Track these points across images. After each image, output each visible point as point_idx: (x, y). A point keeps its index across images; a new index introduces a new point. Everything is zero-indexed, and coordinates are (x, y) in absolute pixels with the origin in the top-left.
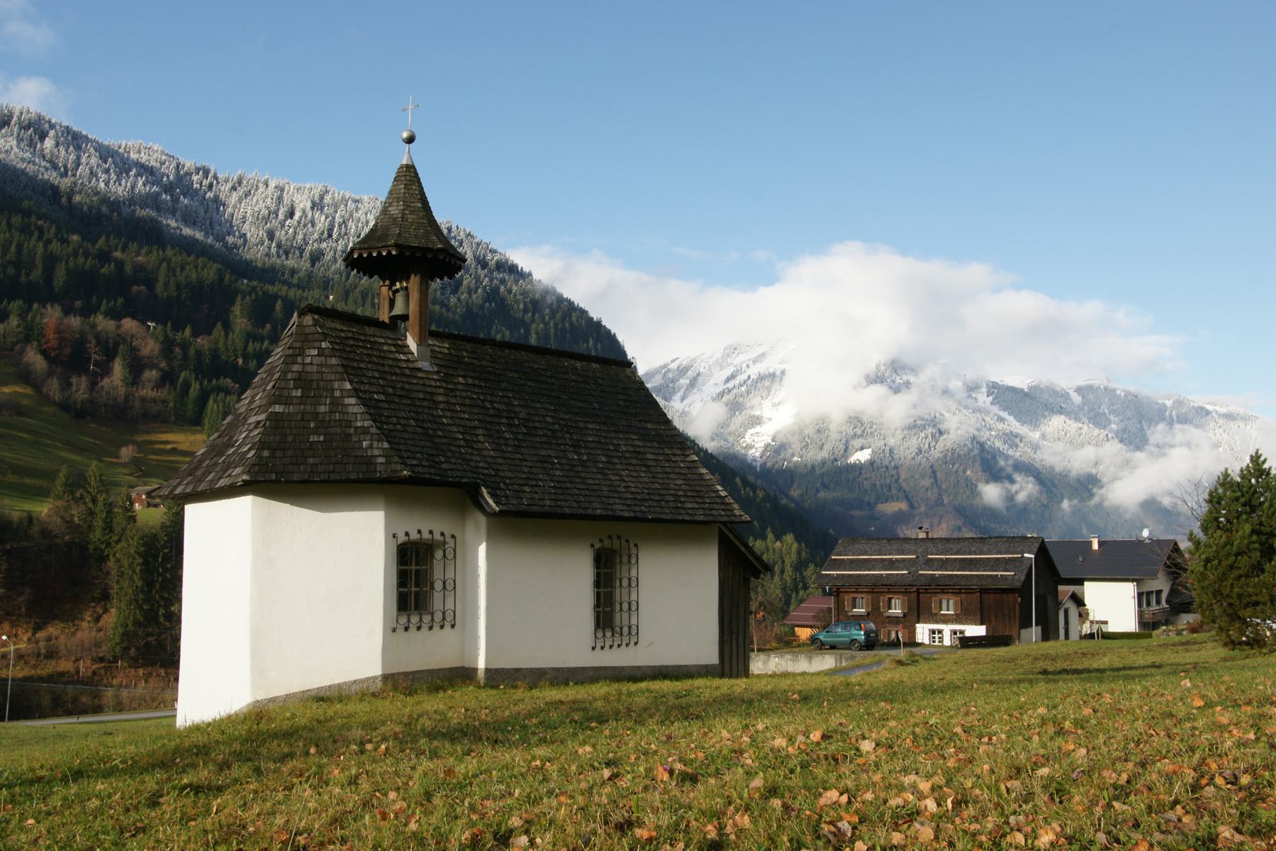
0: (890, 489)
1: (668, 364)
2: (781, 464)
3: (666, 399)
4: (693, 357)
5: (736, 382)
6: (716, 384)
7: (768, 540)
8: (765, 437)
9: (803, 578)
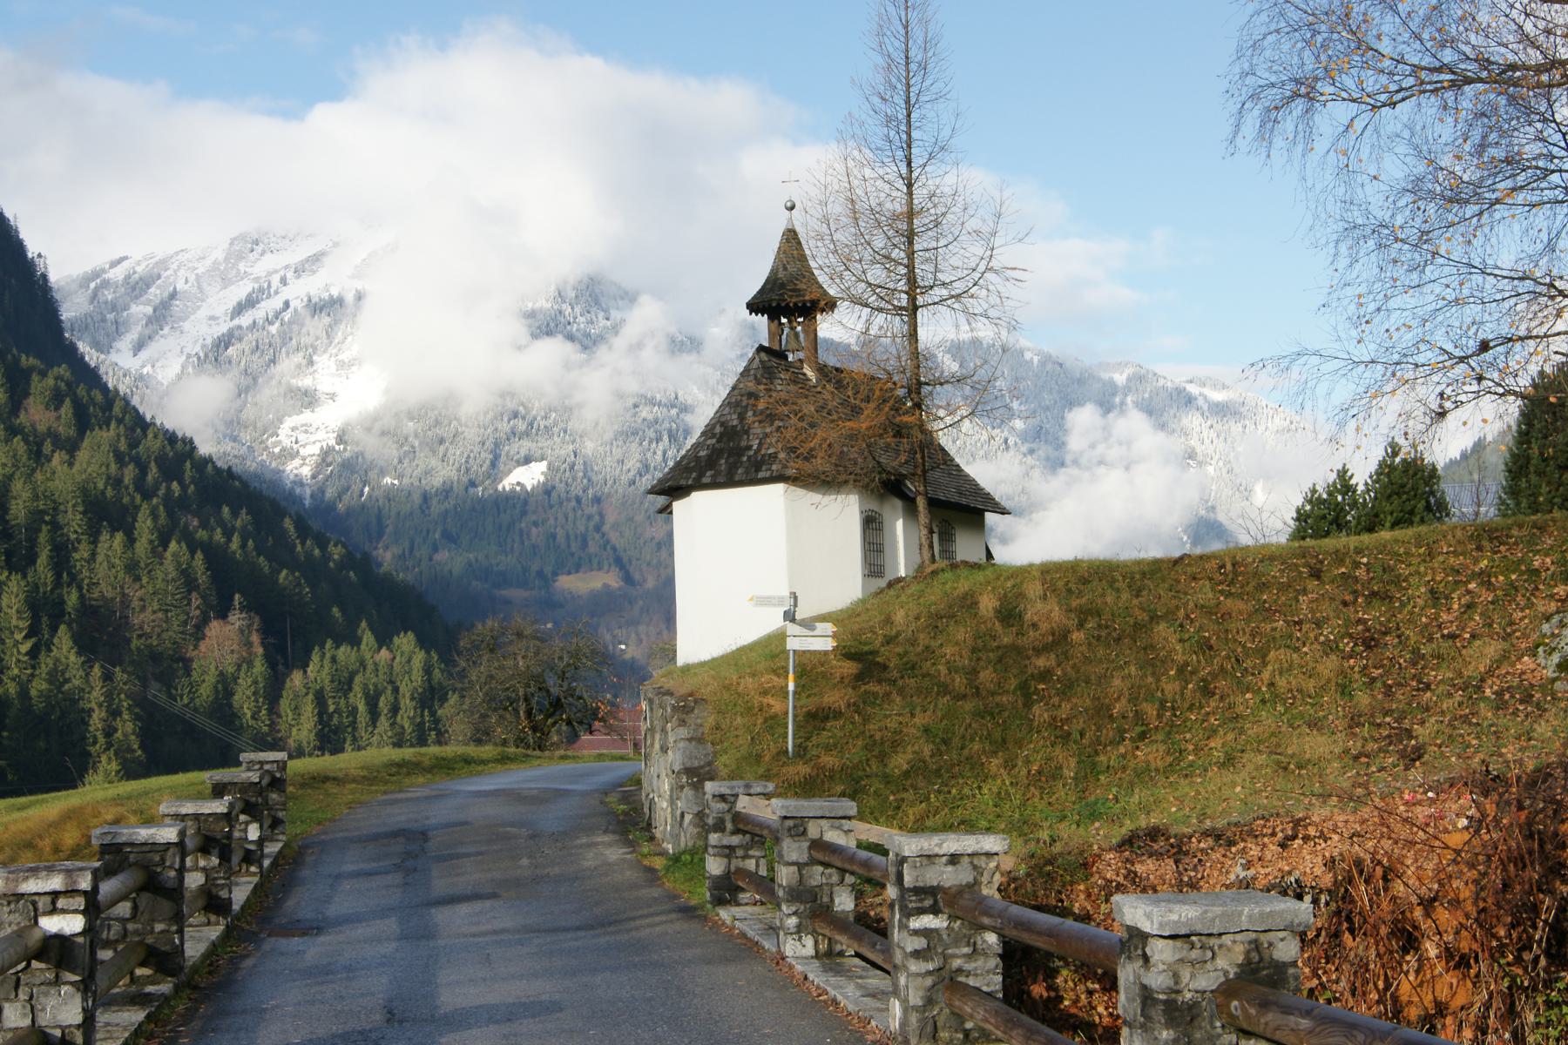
0: (584, 544)
1: (104, 271)
2: (357, 493)
3: (99, 346)
4: (160, 256)
5: (259, 313)
6: (213, 318)
7: (363, 647)
8: (321, 435)
9: (437, 721)
